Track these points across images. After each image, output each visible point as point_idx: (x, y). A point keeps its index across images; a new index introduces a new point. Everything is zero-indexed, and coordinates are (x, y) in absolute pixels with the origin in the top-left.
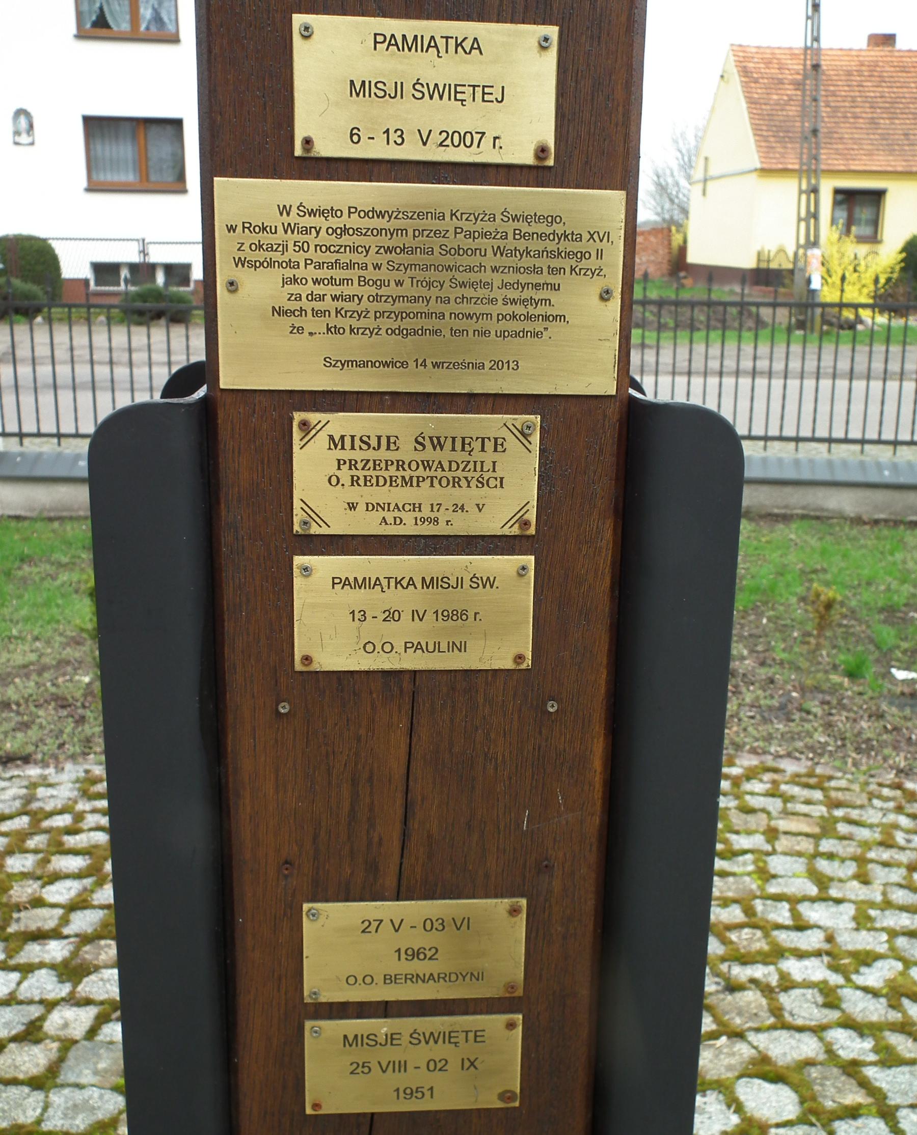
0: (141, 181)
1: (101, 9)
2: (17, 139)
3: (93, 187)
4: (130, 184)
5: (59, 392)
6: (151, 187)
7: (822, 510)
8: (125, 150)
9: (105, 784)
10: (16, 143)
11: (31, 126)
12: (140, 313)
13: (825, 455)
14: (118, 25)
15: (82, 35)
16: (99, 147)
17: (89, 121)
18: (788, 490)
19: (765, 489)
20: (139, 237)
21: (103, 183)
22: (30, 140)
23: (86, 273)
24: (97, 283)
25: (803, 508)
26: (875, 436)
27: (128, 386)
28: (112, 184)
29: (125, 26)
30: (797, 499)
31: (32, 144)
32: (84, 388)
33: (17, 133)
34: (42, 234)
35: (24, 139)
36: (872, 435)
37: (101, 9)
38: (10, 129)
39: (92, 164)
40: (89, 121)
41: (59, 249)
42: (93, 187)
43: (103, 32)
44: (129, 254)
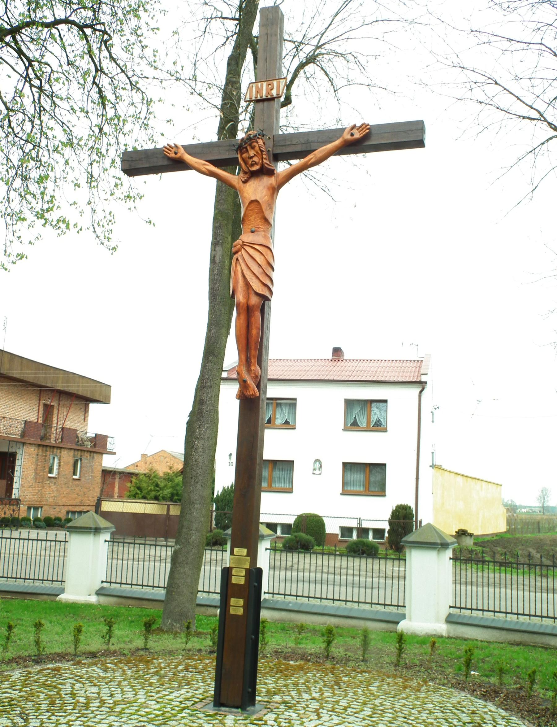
0: (366, 490)
1: (355, 418)
2: (315, 472)
3: (344, 493)
4: (361, 492)
5: (373, 590)
6: (370, 493)
7: (549, 645)
8: (359, 477)
9: (216, 654)
10: (313, 474)
11: (321, 467)
12: (355, 552)
13: (283, 599)
14: (362, 424)
15: (346, 429)
16: (349, 475)
17: (345, 464)
18: (535, 636)
19: (526, 635)
20: (358, 517)
21: (348, 491)
22: (320, 472)
23: (338, 531)
24: (341, 537)
25: (542, 644)
26: (46, 579)
27: (358, 586)
28: (353, 491)
29: (365, 425)
30: (539, 639)
31: (320, 474)
32: (369, 588)
33: (315, 469)
34: (320, 515)
35: (317, 472)
36: (18, 576)
37: (355, 418)
38: (312, 468)
39: (344, 484)
40: (345, 464)
41: (326, 520)
42: (344, 493)
43: (355, 428)
44: (354, 524)
